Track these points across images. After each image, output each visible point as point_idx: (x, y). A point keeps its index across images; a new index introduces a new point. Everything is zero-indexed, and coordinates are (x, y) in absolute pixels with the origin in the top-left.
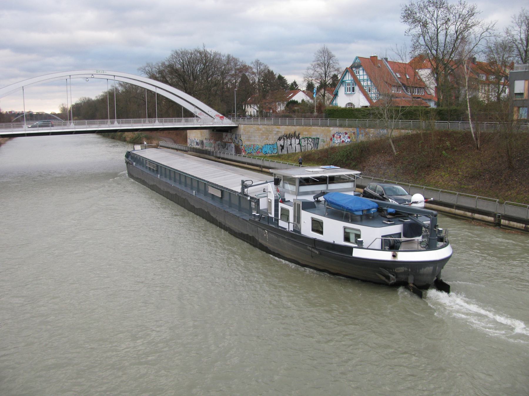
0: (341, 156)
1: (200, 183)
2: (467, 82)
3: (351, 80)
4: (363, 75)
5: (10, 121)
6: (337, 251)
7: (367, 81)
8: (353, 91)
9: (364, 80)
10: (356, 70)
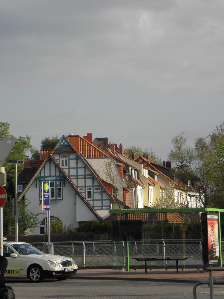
0: (182, 167)
1: (77, 137)
2: (111, 207)
3: (55, 176)
4: (77, 168)
5: (132, 267)
6: (167, 242)
7: (85, 178)
8: (60, 195)
9: (77, 177)
10: (61, 159)
